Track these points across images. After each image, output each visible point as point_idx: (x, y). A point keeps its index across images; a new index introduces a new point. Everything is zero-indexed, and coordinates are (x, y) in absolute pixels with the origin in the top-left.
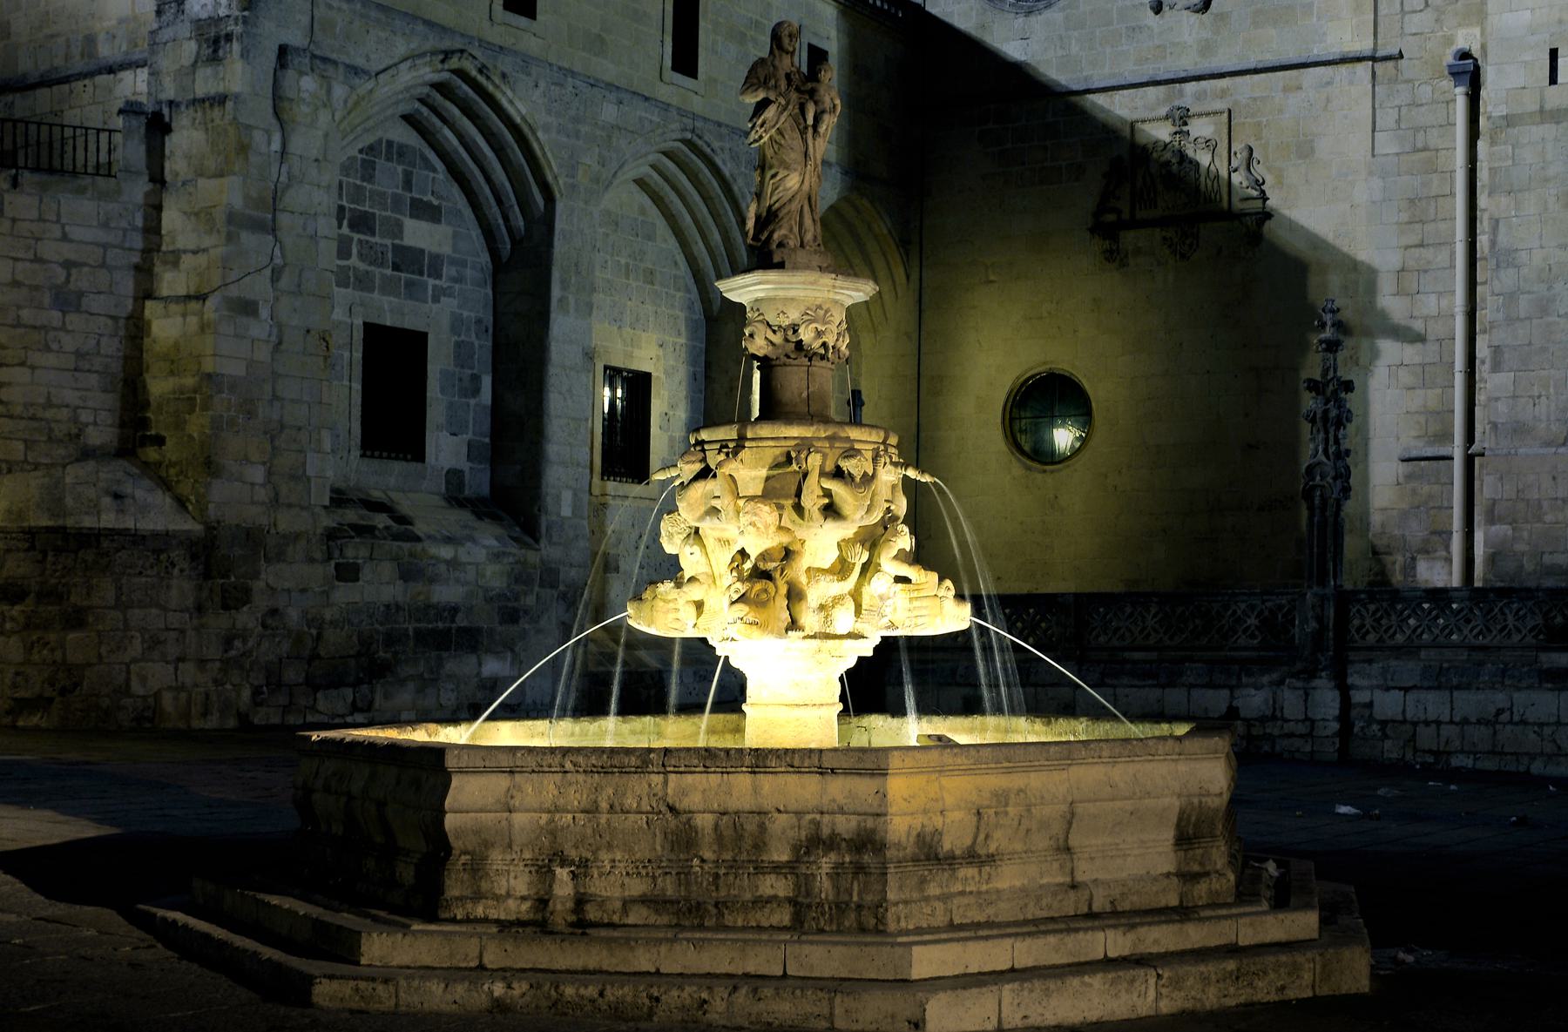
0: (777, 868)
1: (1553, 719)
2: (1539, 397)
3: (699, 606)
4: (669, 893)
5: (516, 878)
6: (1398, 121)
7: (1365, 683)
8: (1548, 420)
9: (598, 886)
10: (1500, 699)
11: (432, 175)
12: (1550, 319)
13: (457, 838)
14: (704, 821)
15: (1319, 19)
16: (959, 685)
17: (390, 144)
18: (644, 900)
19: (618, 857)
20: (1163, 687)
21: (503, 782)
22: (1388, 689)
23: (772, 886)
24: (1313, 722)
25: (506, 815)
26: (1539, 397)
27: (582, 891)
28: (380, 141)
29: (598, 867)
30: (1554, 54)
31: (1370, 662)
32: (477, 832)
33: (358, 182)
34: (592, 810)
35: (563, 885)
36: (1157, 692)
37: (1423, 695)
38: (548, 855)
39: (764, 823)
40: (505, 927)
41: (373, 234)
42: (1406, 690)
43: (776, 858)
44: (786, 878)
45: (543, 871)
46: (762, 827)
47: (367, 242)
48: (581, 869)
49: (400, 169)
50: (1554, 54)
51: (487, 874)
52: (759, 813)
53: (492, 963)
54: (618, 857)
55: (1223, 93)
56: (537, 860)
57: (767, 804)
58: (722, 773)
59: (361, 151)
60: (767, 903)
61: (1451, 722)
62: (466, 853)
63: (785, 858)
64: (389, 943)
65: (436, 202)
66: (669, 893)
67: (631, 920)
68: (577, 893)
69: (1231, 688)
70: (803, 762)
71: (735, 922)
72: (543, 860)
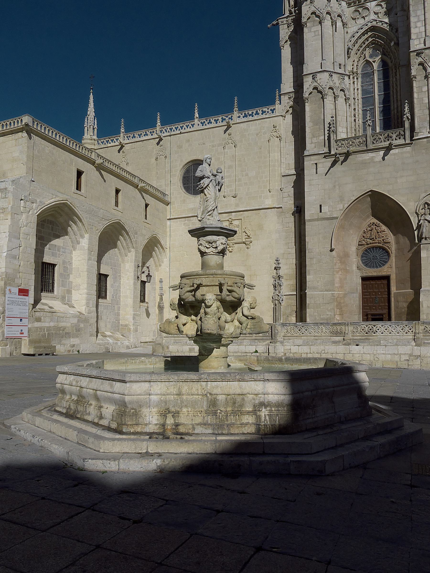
0: (248, 413)
1: (335, 352)
2: (319, 281)
3: (184, 325)
4: (209, 422)
5: (152, 417)
6: (282, 221)
7: (289, 344)
8: (321, 286)
9: (182, 419)
10: (322, 347)
11: (58, 228)
12: (321, 264)
13: (129, 404)
14: (221, 398)
15: (263, 199)
16: (188, 345)
17: (48, 220)
18: (200, 424)
19: (190, 410)
20: (239, 345)
21: (147, 385)
22: (294, 346)
23: (247, 419)
24: (276, 353)
25: (148, 396)
26: (319, 281)
27: (177, 421)
28: (46, 219)
29: (183, 414)
30: (321, 206)
31: (290, 339)
32: (137, 402)
33: (40, 229)
34: (179, 394)
35: (170, 421)
36: (237, 347)
37: (303, 347)
38: (164, 409)
39: (244, 398)
40: (151, 435)
41: (44, 241)
42: (299, 346)
43: (247, 409)
44: (252, 416)
45: (164, 414)
46: (243, 399)
47: (42, 243)
48: (176, 414)
49: (50, 226)
50: (321, 206)
51: (141, 416)
52: (242, 395)
53: (151, 451)
54: (190, 410)
55: (241, 215)
56: (160, 411)
57: (245, 392)
58: (228, 381)
59: (41, 221)
60: (246, 425)
61: (310, 353)
62: (133, 409)
63: (251, 409)
64: (111, 444)
65: (59, 234)
66: (209, 422)
67: (196, 431)
68: (175, 423)
69: (256, 346)
70: (257, 378)
71: (235, 431)
72: (162, 411)
